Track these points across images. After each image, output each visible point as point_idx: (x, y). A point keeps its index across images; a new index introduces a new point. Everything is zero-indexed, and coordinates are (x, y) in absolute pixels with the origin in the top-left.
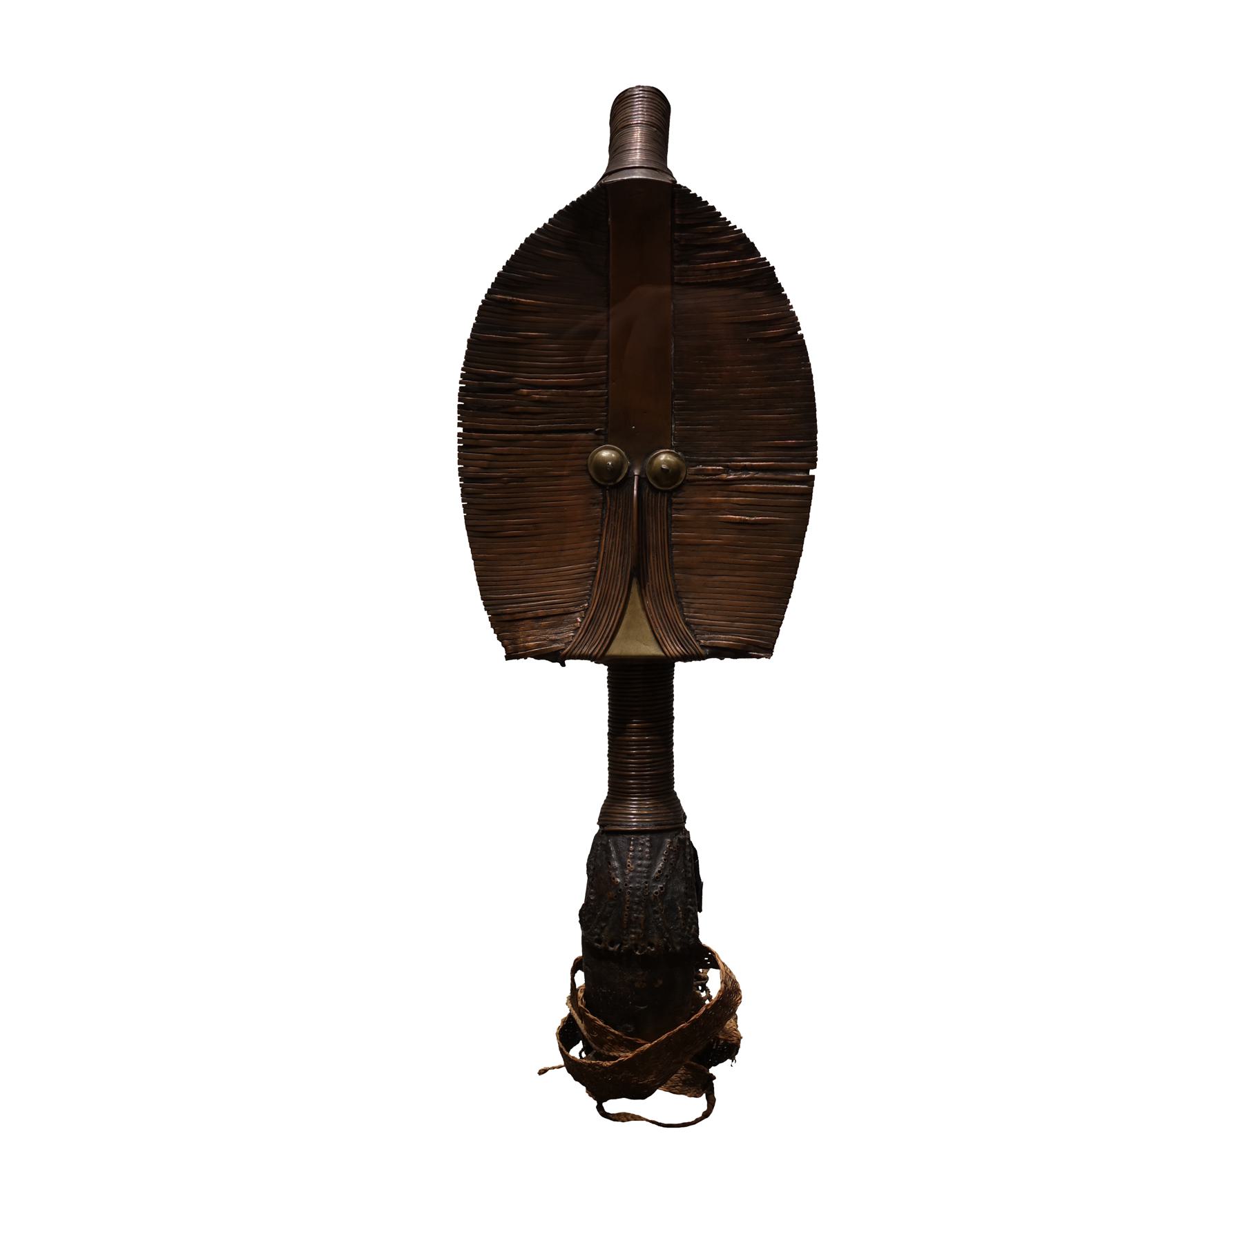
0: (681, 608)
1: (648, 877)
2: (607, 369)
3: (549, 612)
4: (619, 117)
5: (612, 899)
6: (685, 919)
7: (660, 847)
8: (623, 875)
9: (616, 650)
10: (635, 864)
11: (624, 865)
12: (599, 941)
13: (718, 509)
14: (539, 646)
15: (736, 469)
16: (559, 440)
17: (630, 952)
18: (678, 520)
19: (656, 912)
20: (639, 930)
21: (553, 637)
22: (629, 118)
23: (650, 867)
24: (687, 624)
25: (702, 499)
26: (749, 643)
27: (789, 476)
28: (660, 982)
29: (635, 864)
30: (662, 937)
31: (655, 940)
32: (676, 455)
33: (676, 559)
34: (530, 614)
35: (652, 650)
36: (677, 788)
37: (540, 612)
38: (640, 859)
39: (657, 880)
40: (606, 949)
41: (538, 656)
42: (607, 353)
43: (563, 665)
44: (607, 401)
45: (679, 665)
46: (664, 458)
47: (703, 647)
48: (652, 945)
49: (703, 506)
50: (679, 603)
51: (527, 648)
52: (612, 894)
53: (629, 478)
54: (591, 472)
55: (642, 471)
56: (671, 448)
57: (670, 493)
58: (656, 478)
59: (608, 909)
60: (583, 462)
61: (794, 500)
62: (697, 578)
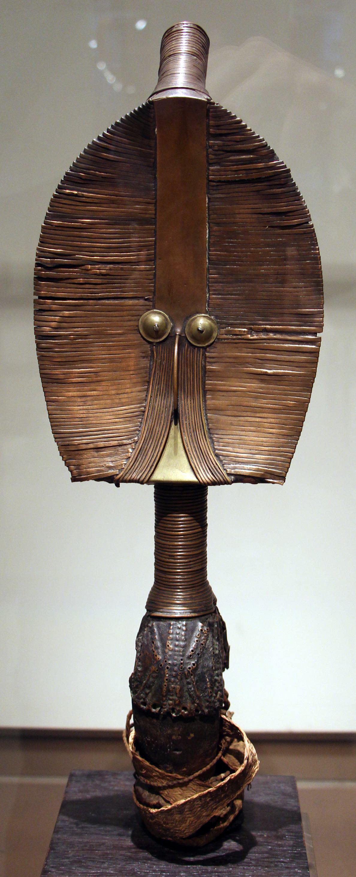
0: (213, 442)
1: (183, 656)
2: (155, 248)
3: (107, 444)
4: (167, 48)
5: (154, 672)
6: (212, 688)
7: (193, 630)
8: (164, 652)
9: (160, 475)
10: (252, 480)
11: (164, 645)
12: (145, 704)
13: (244, 362)
14: (99, 471)
15: (258, 331)
16: (116, 305)
17: (168, 714)
18: (212, 371)
19: (189, 683)
20: (175, 697)
21: (111, 464)
22: (177, 47)
23: (185, 647)
24: (217, 455)
25: (230, 354)
26: (266, 472)
27: (301, 337)
28: (192, 735)
29: (182, 638)
30: (193, 703)
31: (189, 705)
32: (210, 319)
33: (208, 402)
34: (91, 446)
35: (188, 476)
36: (209, 578)
37: (101, 444)
38: (177, 640)
39: (190, 657)
40: (149, 711)
41: (98, 479)
42: (155, 236)
43: (118, 485)
44: (155, 274)
45: (209, 488)
46: (202, 322)
47: (229, 475)
48: (185, 709)
49: (231, 360)
50: (211, 438)
51: (88, 473)
52: (154, 668)
53: (172, 336)
54: (141, 331)
55: (183, 331)
56: (206, 313)
57: (205, 348)
58: (193, 338)
59: (151, 679)
60: (135, 323)
61: (303, 358)
62: (226, 418)
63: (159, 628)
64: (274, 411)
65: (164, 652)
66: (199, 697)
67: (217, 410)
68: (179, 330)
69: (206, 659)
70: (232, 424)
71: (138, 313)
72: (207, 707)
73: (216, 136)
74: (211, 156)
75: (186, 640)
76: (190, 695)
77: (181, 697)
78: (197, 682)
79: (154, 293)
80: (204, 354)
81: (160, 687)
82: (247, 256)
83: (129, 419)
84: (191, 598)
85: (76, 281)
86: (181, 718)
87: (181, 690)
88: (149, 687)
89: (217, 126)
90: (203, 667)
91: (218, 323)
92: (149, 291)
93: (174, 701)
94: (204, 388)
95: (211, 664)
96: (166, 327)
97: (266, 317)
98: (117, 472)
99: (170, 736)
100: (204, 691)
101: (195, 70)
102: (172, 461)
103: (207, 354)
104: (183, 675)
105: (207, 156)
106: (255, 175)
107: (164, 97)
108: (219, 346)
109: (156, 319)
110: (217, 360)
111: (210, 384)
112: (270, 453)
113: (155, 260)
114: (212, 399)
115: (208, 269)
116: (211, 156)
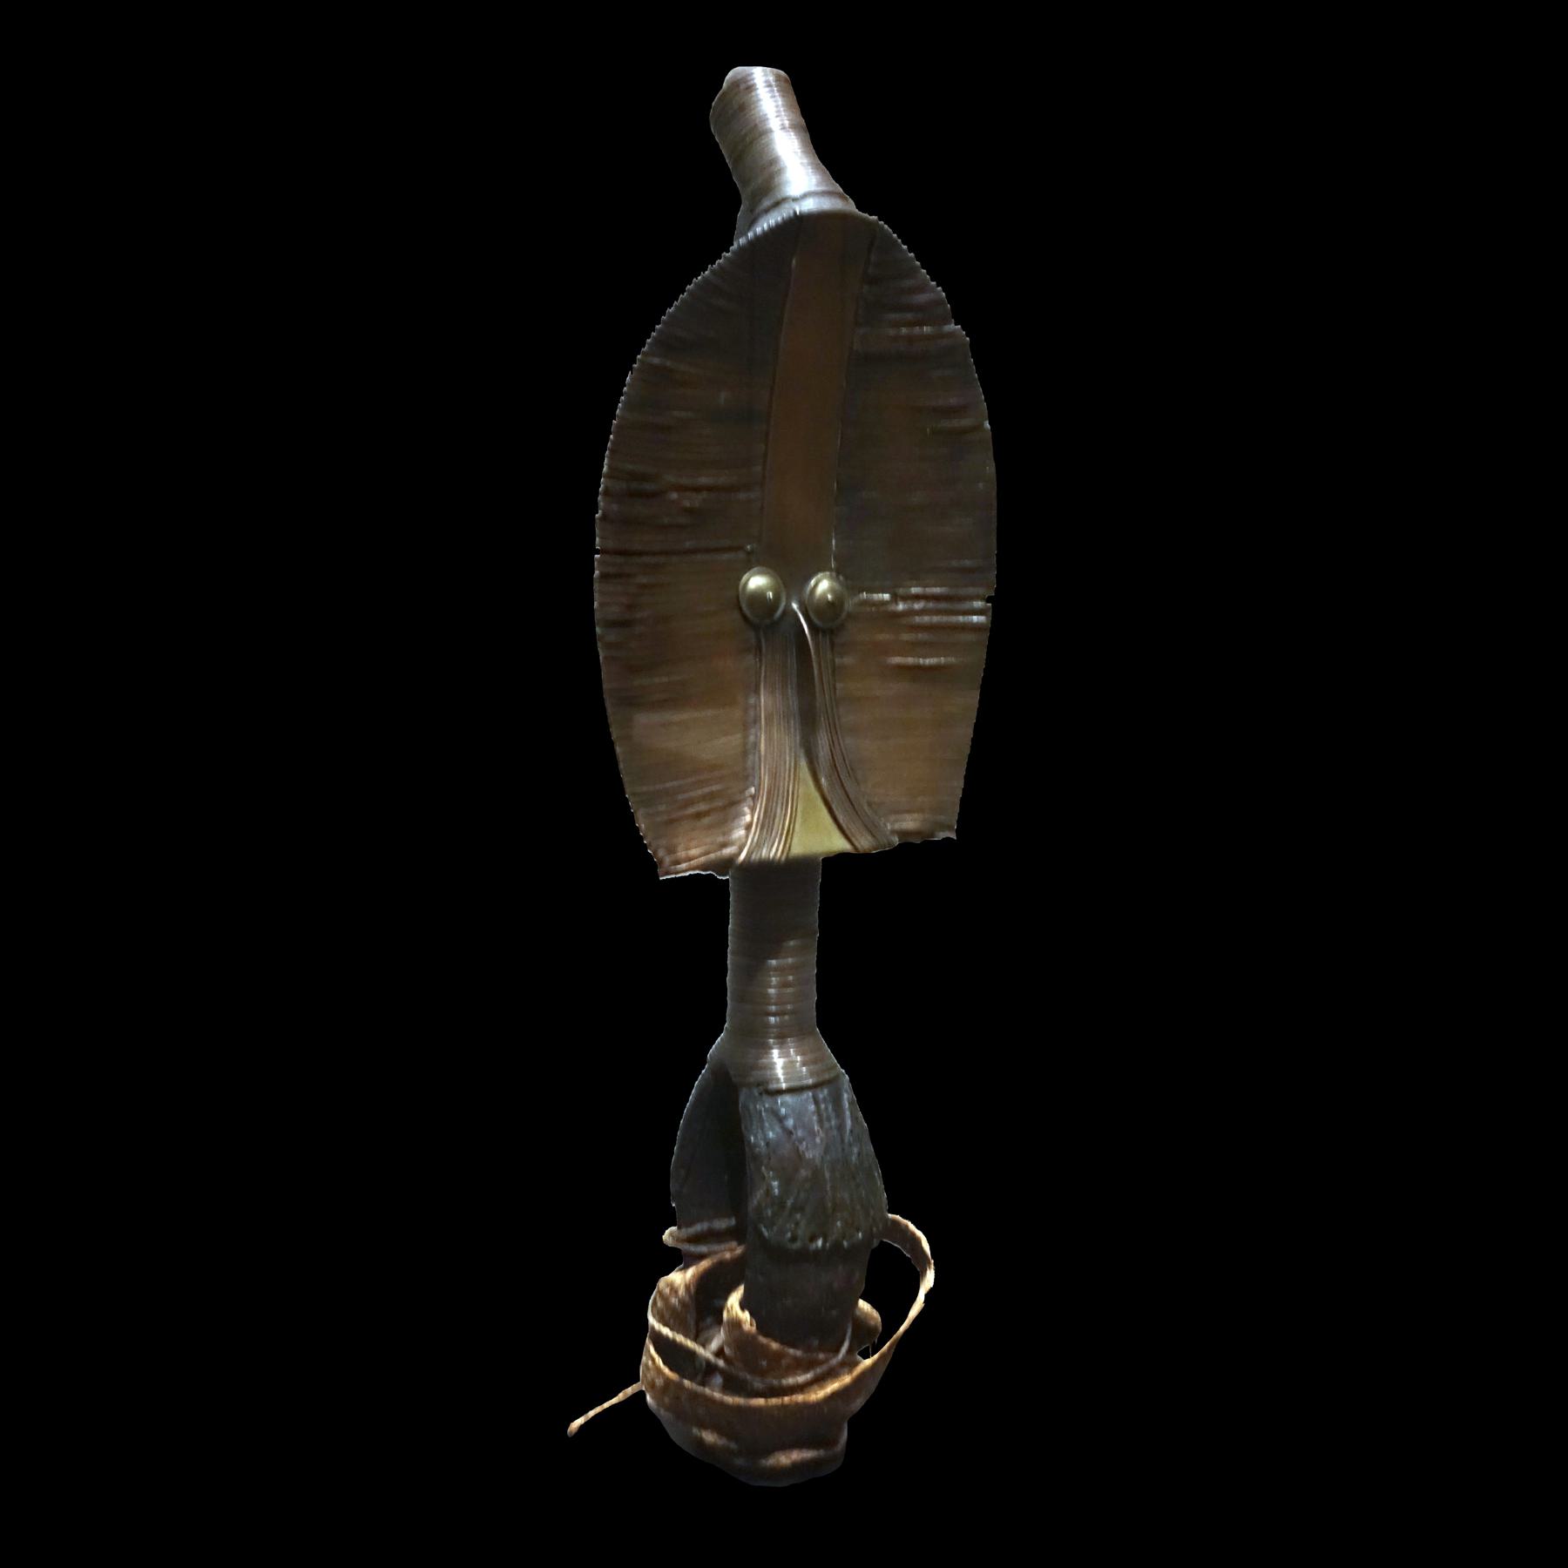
17: (837, 1246)
46: (823, 586)
52: (803, 1173)
68: (795, 606)
88: (798, 1208)
97: (916, 578)
109: (757, 582)
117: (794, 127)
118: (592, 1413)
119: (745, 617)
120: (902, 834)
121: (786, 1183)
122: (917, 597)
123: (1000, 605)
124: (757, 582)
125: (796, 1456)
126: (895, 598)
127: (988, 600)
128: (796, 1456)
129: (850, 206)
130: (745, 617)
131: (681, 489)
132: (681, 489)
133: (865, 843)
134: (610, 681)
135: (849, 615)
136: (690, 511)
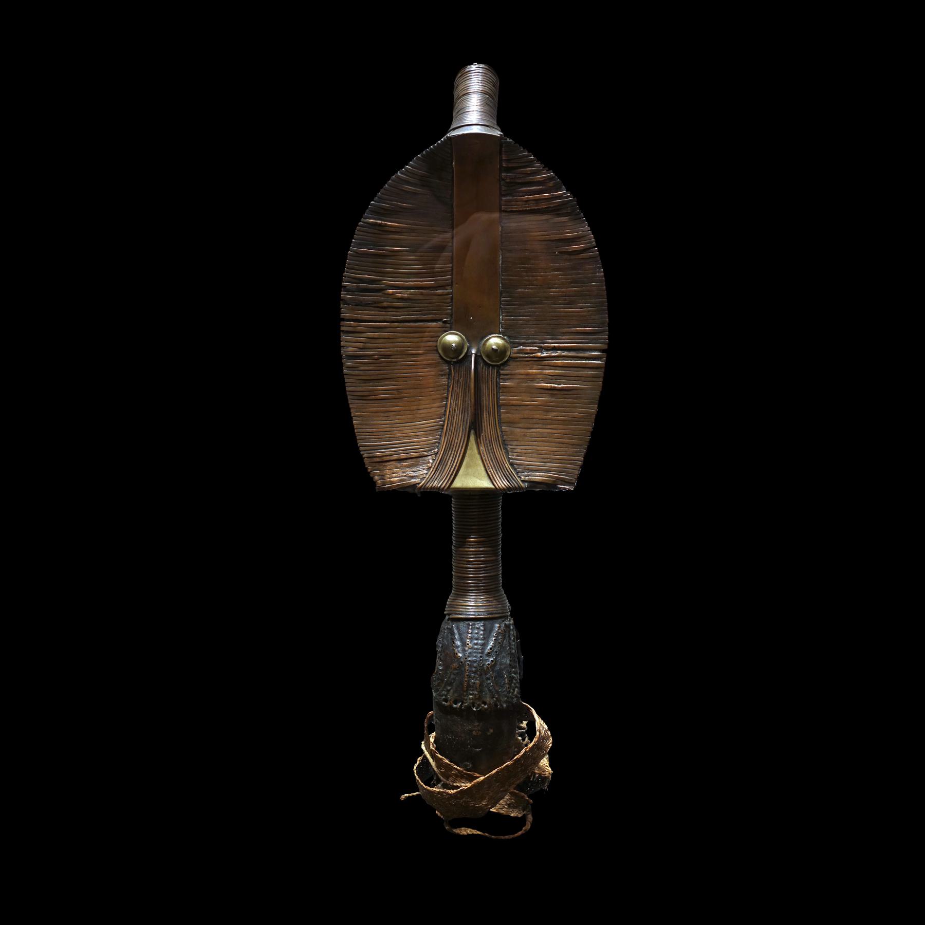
0: (507, 452)
1: (482, 653)
2: (452, 275)
3: (409, 455)
5: (455, 669)
6: (510, 684)
7: (491, 630)
8: (464, 651)
11: (464, 644)
12: (446, 700)
15: (547, 349)
16: (416, 327)
17: (469, 708)
18: (505, 387)
19: (488, 679)
20: (476, 692)
23: (484, 645)
24: (512, 464)
25: (522, 371)
26: (558, 479)
27: (588, 354)
28: (492, 731)
31: (488, 700)
32: (503, 339)
33: (503, 416)
34: (394, 457)
37: (402, 456)
39: (489, 655)
40: (451, 706)
42: (452, 263)
46: (495, 341)
47: (523, 481)
48: (485, 703)
50: (505, 449)
52: (455, 665)
53: (468, 356)
56: (500, 333)
58: (488, 356)
59: (452, 676)
60: (434, 344)
62: (518, 430)
63: (458, 628)
64: (564, 422)
65: (464, 651)
66: (497, 692)
67: (511, 423)
68: (473, 351)
69: (504, 657)
70: (525, 436)
71: (436, 334)
72: (506, 702)
73: (508, 170)
74: (503, 188)
75: (484, 639)
76: (490, 691)
77: (481, 692)
78: (496, 677)
79: (451, 315)
80: (499, 374)
81: (461, 683)
82: (536, 280)
83: (430, 433)
84: (488, 601)
85: (379, 305)
86: (481, 713)
87: (481, 685)
88: (451, 684)
89: (508, 161)
90: (501, 664)
91: (511, 342)
92: (447, 314)
93: (475, 695)
94: (500, 419)
95: (508, 662)
96: (463, 347)
97: (554, 336)
98: (417, 480)
99: (471, 731)
100: (502, 687)
101: (487, 108)
102: (470, 470)
103: (502, 372)
104: (482, 671)
105: (500, 188)
106: (543, 206)
107: (461, 133)
108: (512, 364)
109: (452, 338)
110: (511, 377)
111: (503, 399)
112: (561, 461)
113: (451, 285)
114: (507, 413)
115: (501, 293)
116: (503, 188)
117: (484, 93)
118: (511, 836)
119: (440, 356)
120: (530, 482)
121: (447, 667)
122: (555, 349)
123: (610, 353)
124: (452, 338)
125: (469, 831)
126: (541, 349)
127: (602, 351)
128: (469, 831)
129: (497, 133)
130: (440, 356)
131: (393, 287)
132: (393, 287)
133: (502, 483)
134: (351, 386)
135: (511, 358)
136: (402, 299)
